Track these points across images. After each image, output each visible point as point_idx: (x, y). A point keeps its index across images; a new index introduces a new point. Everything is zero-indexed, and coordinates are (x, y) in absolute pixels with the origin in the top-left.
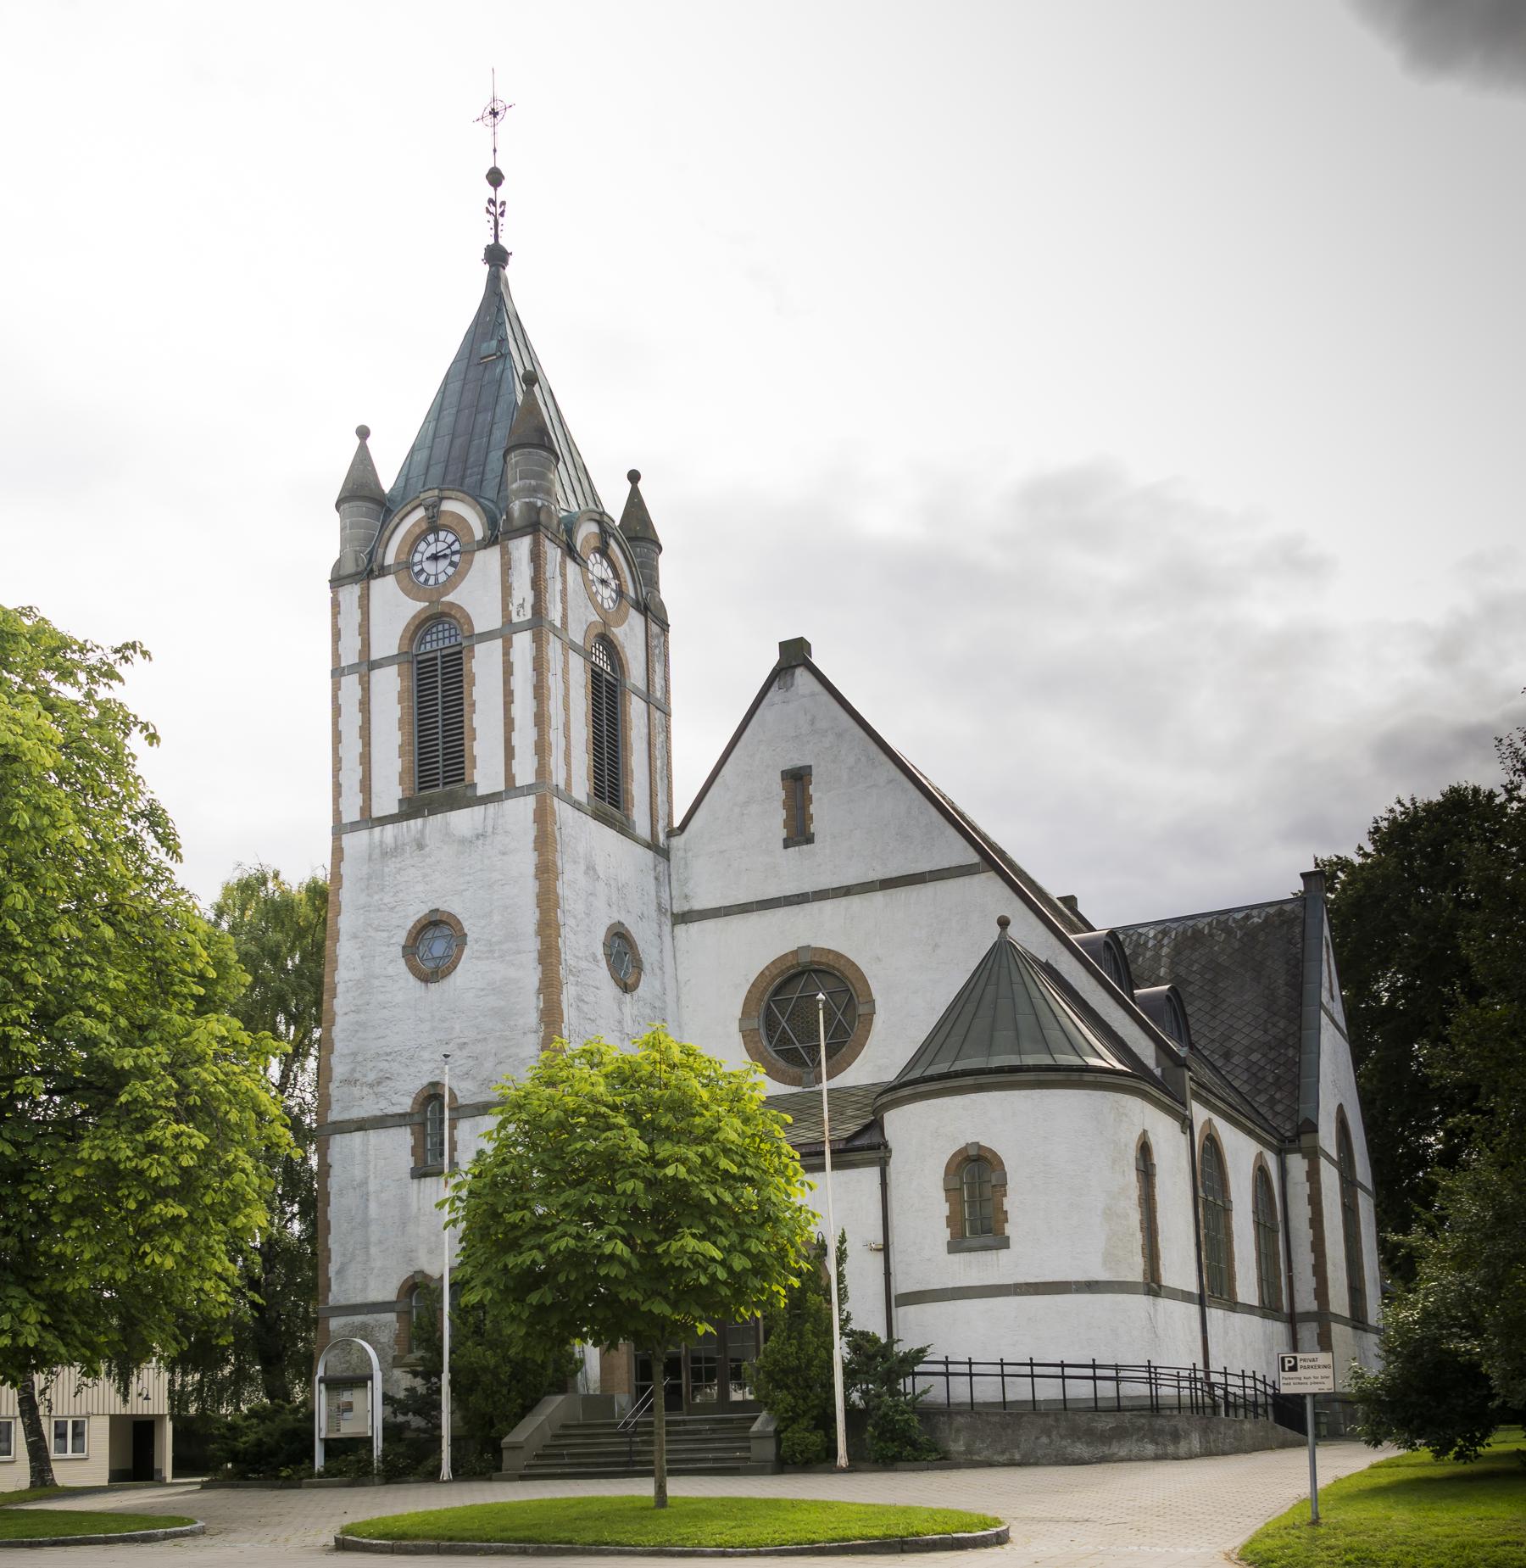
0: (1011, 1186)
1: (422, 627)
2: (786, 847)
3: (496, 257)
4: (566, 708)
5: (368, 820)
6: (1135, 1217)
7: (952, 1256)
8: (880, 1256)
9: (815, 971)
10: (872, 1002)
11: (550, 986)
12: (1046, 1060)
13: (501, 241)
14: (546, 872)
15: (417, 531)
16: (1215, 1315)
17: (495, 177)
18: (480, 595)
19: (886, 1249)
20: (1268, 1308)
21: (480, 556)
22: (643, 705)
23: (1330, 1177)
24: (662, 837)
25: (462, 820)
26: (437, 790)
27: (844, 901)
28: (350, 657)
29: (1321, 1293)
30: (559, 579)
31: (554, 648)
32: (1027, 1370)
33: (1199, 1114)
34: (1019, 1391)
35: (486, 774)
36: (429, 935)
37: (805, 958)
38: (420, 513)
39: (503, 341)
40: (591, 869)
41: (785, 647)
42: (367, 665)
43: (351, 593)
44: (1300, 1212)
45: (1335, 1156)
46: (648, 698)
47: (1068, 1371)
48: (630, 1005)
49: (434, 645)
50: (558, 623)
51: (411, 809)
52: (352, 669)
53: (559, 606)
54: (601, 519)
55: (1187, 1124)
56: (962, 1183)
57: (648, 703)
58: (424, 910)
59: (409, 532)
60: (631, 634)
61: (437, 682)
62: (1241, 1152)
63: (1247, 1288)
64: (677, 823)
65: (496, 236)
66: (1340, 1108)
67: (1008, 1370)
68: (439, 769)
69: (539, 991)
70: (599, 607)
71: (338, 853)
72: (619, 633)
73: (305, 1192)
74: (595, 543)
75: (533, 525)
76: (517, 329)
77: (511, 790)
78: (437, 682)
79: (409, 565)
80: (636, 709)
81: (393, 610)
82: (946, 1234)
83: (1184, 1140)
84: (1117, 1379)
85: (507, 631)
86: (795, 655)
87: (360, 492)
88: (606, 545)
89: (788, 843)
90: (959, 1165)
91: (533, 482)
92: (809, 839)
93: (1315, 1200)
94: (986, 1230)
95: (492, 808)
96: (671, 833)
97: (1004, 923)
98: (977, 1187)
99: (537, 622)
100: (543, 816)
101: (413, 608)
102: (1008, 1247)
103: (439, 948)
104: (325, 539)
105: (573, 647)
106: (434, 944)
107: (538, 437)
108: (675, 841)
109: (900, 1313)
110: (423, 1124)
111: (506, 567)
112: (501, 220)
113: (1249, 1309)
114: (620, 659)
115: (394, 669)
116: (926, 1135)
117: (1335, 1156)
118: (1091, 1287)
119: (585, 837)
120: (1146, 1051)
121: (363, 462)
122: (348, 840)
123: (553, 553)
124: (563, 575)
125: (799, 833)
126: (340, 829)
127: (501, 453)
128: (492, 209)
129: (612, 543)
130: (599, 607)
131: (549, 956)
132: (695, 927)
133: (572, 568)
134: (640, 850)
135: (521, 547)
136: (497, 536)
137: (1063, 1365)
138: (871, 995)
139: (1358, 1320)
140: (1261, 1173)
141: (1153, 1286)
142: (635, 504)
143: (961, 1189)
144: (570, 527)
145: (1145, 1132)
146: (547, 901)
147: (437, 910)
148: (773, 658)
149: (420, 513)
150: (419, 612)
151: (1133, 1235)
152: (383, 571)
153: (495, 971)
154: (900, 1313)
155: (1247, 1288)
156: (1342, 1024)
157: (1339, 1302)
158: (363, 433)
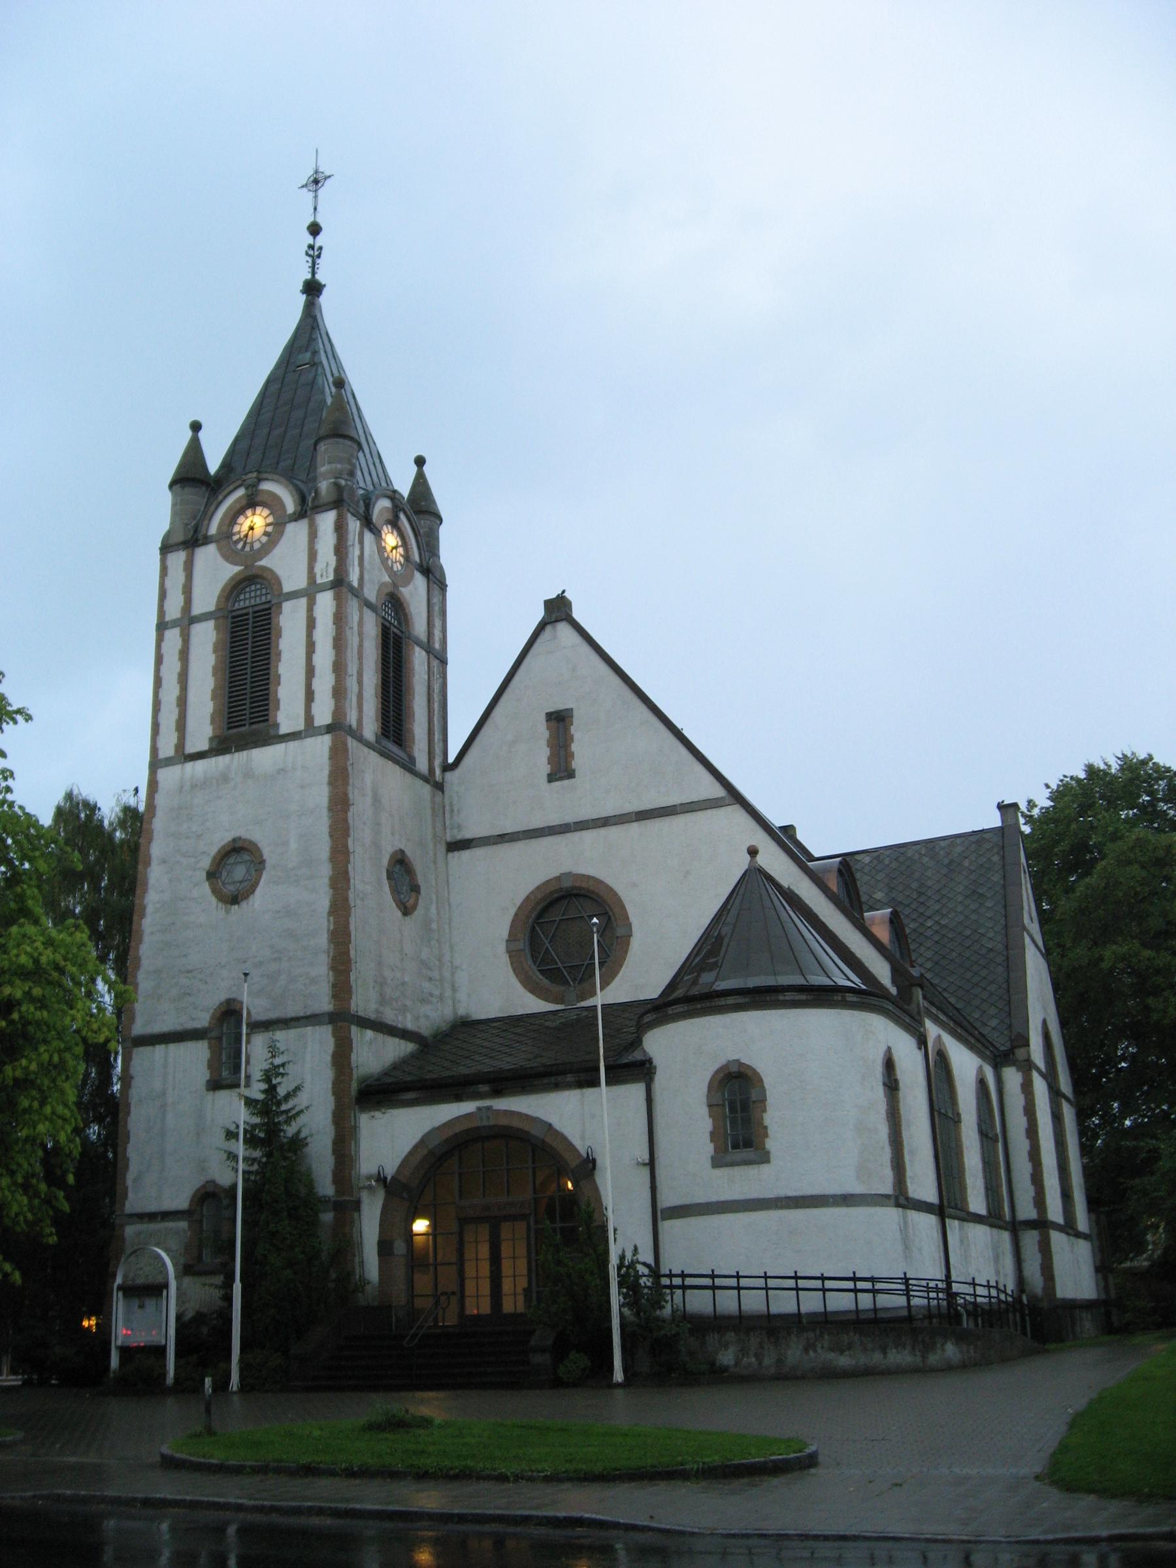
0: (770, 1100)
1: (236, 587)
2: (550, 781)
3: (313, 289)
4: (360, 658)
5: (184, 756)
6: (883, 1131)
7: (718, 1172)
8: (646, 1172)
9: (577, 896)
10: (629, 926)
11: (340, 908)
12: (798, 980)
13: (317, 277)
14: (340, 804)
15: (238, 506)
16: (953, 1225)
17: (315, 230)
18: (289, 564)
19: (651, 1164)
20: (993, 1219)
21: (291, 528)
22: (424, 653)
23: (1040, 1086)
24: (438, 771)
25: (264, 757)
26: (243, 729)
27: (603, 831)
28: (174, 611)
29: (1040, 1201)
30: (357, 546)
31: (353, 606)
32: (791, 1283)
33: (932, 1030)
34: (784, 1304)
35: (288, 717)
36: (231, 860)
37: (567, 884)
38: (241, 492)
39: (315, 353)
40: (376, 800)
41: (549, 604)
42: (188, 620)
43: (177, 559)
44: (1017, 1122)
45: (1043, 1070)
46: (428, 649)
47: (829, 1284)
48: (410, 925)
49: (250, 600)
50: (355, 584)
51: (222, 745)
52: (175, 623)
53: (357, 569)
54: (393, 496)
55: (922, 1041)
56: (724, 1100)
57: (428, 652)
58: (228, 837)
59: (230, 508)
60: (416, 592)
61: (248, 633)
62: (965, 1064)
63: (977, 1203)
64: (451, 760)
65: (314, 273)
66: (1044, 1022)
67: (772, 1283)
68: (247, 713)
69: (330, 913)
70: (390, 570)
71: (153, 785)
72: (405, 592)
73: (107, 1108)
74: (390, 516)
75: (338, 503)
76: (326, 342)
77: (310, 729)
78: (248, 633)
79: (230, 535)
80: (418, 659)
81: (213, 572)
82: (709, 1148)
83: (919, 1056)
84: (874, 1291)
85: (311, 592)
86: (558, 610)
87: (191, 477)
88: (397, 517)
89: (551, 778)
90: (721, 1081)
91: (339, 466)
92: (571, 775)
93: (1030, 1111)
94: (748, 1144)
95: (292, 745)
96: (447, 768)
97: (753, 852)
98: (738, 1105)
99: (339, 583)
100: (338, 754)
101: (231, 570)
102: (768, 1161)
103: (239, 872)
104: (158, 512)
105: (369, 605)
106: (235, 869)
107: (341, 426)
108: (448, 775)
109: (666, 1226)
110: (220, 1039)
111: (313, 535)
112: (318, 261)
113: (977, 1219)
114: (405, 615)
115: (211, 624)
116: (686, 1052)
117: (1043, 1070)
118: (847, 1200)
119: (376, 775)
120: (882, 970)
121: (194, 452)
122: (163, 774)
123: (354, 525)
124: (361, 542)
125: (561, 768)
126: (156, 764)
127: (313, 441)
128: (311, 252)
129: (402, 516)
130: (390, 570)
131: (340, 881)
132: (466, 855)
133: (368, 537)
134: (419, 783)
135: (327, 521)
136: (307, 509)
137: (823, 1278)
138: (628, 918)
139: (1069, 1227)
140: (982, 1083)
141: (901, 1199)
142: (421, 483)
143: (723, 1105)
144: (368, 503)
145: (889, 1049)
146: (340, 830)
147: (240, 838)
148: (539, 614)
149: (241, 492)
150: (236, 575)
151: (883, 1148)
152: (207, 540)
153: (291, 897)
154: (666, 1226)
155: (977, 1203)
156: (1040, 943)
157: (1055, 1212)
158: (196, 427)
